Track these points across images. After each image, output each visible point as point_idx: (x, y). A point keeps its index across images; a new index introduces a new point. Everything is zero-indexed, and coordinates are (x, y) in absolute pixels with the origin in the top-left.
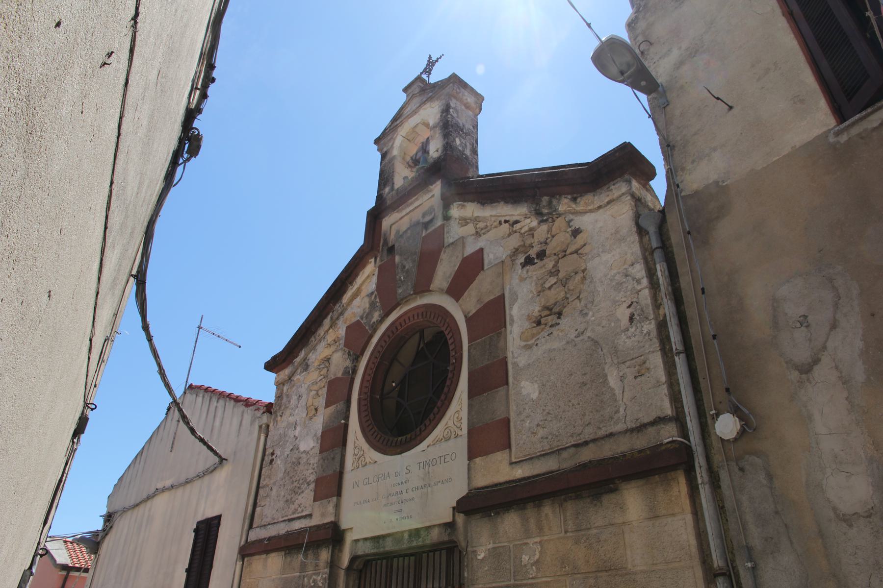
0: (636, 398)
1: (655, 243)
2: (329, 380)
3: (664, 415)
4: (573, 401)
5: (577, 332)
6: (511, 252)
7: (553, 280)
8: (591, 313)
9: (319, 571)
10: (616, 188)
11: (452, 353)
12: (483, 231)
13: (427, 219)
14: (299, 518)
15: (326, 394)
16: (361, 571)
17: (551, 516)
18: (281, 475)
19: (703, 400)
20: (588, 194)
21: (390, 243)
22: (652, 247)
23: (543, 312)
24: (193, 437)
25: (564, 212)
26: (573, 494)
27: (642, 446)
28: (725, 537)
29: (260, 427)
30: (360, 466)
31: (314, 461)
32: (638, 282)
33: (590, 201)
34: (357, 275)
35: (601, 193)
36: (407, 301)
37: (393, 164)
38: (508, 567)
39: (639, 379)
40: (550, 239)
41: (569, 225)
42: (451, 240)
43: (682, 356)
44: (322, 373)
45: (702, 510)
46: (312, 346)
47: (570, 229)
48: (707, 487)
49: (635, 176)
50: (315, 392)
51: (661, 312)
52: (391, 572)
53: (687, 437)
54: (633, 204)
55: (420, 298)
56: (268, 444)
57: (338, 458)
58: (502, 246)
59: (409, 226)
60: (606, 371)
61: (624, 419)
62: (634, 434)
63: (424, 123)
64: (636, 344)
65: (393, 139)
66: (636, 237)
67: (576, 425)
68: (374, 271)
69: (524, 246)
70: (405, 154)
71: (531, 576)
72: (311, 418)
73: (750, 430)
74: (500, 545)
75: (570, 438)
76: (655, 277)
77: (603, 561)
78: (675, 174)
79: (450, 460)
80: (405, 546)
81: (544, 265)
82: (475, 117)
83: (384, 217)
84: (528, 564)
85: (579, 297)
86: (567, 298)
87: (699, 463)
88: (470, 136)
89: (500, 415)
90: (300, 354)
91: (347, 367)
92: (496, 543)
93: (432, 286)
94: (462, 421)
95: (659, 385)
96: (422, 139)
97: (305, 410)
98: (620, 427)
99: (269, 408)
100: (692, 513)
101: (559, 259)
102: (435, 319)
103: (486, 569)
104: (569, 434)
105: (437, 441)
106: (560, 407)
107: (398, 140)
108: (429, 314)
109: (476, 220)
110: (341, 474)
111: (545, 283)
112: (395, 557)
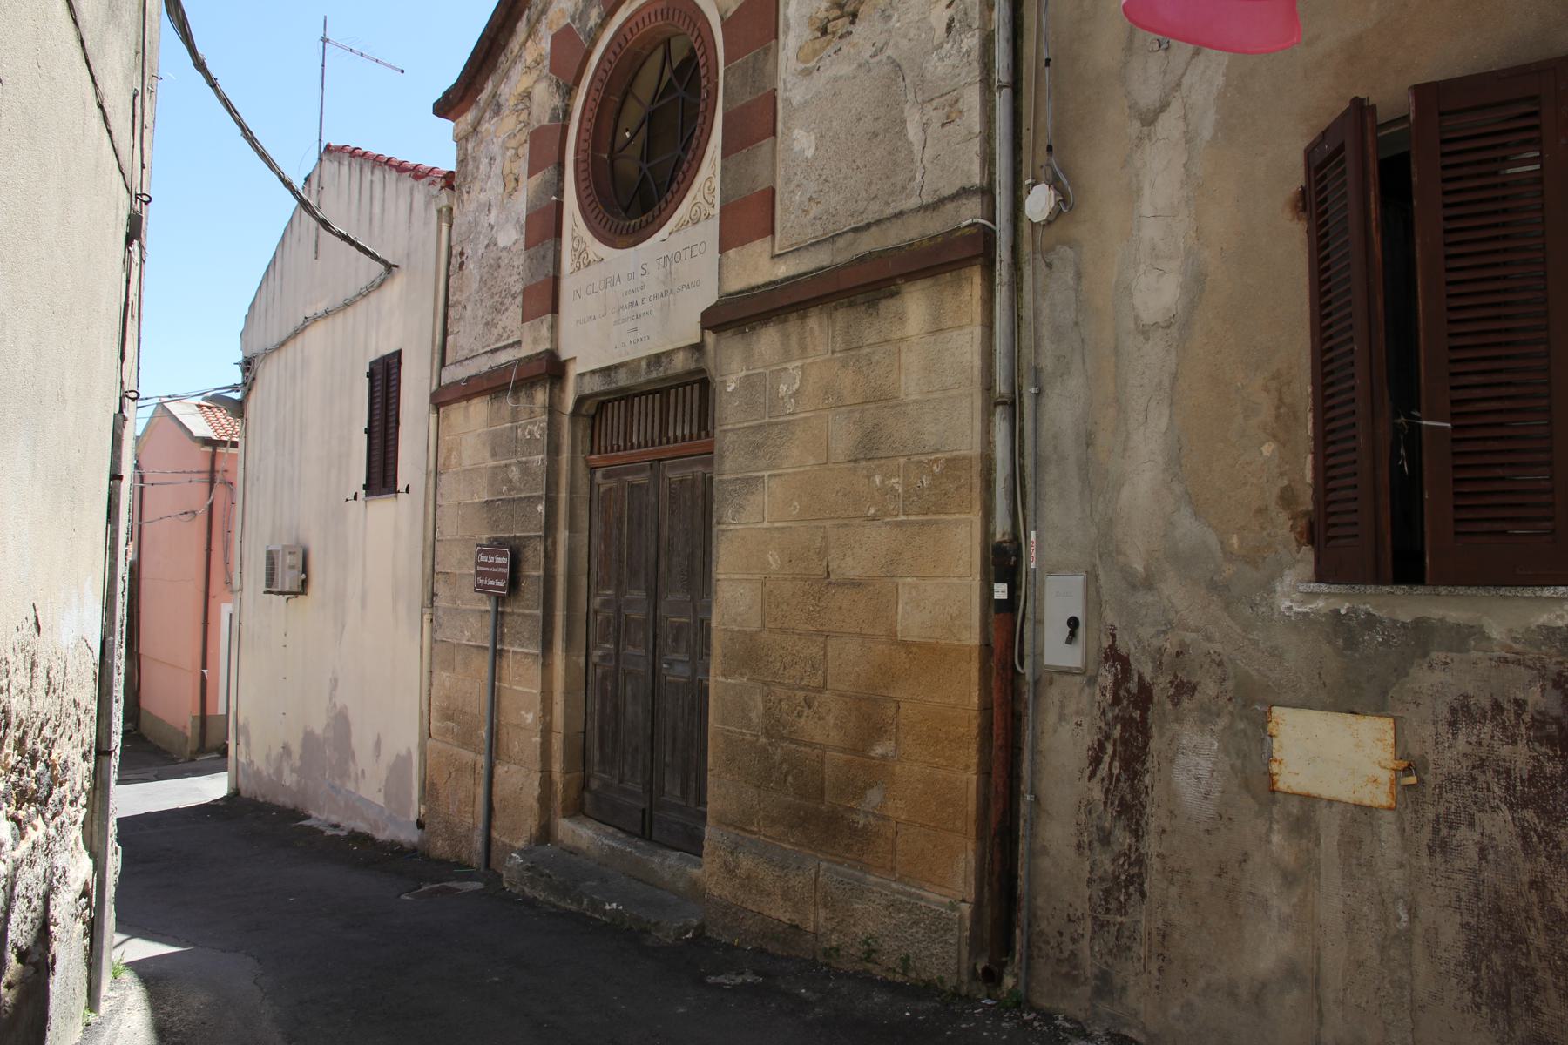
11: (704, 82)
14: (505, 347)
16: (593, 417)
17: (817, 330)
18: (475, 285)
24: (329, 233)
26: (846, 300)
29: (440, 211)
31: (519, 261)
38: (762, 401)
43: (1006, 92)
44: (521, 119)
48: (1004, 289)
50: (513, 151)
60: (906, 114)
62: (928, 212)
72: (510, 195)
74: (753, 372)
80: (642, 379)
91: (555, 109)
92: (749, 370)
97: (501, 182)
98: (914, 202)
99: (449, 180)
110: (556, 280)
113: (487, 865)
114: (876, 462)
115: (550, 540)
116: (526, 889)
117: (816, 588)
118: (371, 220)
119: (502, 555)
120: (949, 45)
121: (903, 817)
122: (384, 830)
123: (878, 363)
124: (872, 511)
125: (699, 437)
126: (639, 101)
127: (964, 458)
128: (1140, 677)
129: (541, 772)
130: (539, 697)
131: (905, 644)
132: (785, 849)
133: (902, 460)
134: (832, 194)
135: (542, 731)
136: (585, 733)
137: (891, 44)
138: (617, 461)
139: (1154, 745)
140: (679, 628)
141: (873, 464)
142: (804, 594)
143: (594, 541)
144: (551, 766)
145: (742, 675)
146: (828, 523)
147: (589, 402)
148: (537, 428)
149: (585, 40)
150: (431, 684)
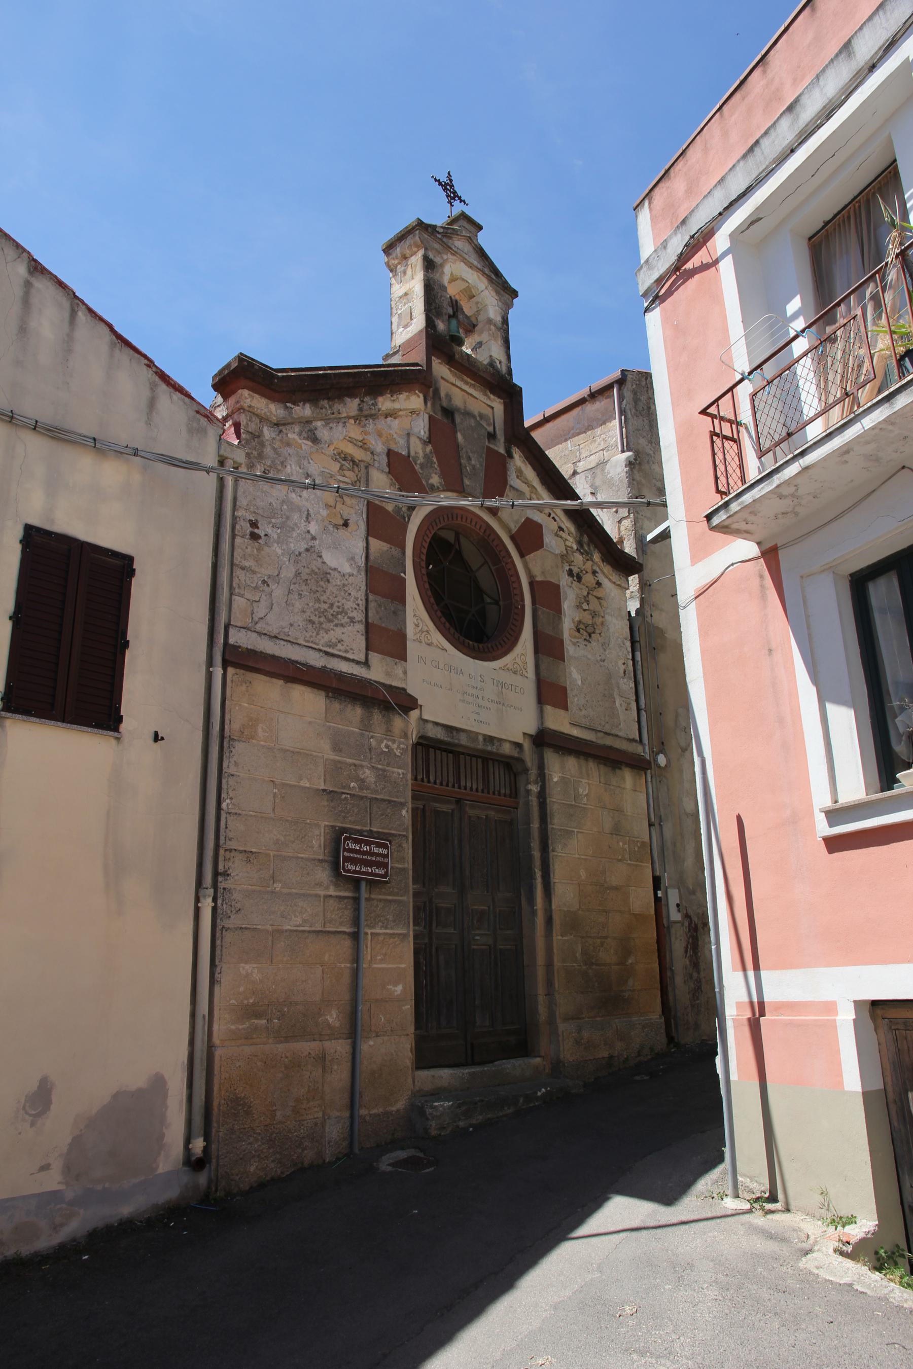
17: (593, 767)
103: (559, 789)
128: (695, 922)
139: (700, 943)
145: (571, 934)
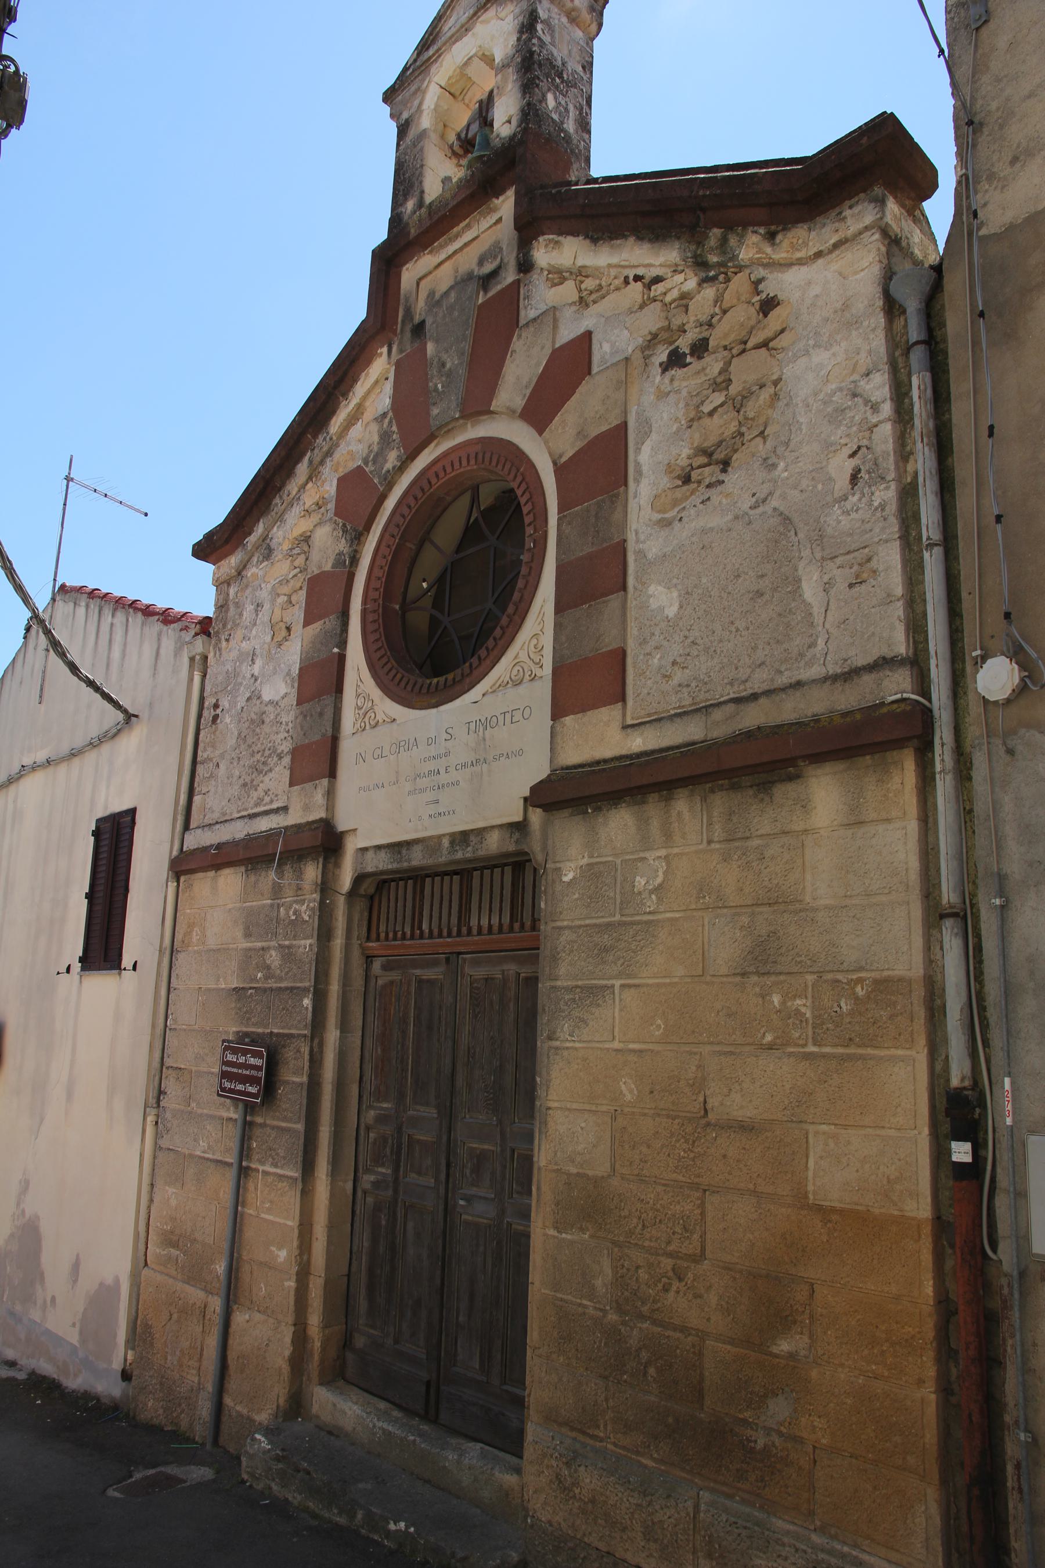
0: (847, 622)
1: (915, 332)
2: (309, 576)
3: (893, 655)
4: (738, 623)
5: (754, 499)
6: (643, 341)
7: (718, 398)
8: (782, 465)
9: (302, 897)
10: (852, 216)
11: (529, 531)
12: (594, 296)
13: (488, 268)
14: (266, 813)
15: (304, 601)
16: (372, 898)
17: (686, 815)
18: (232, 742)
19: (962, 632)
20: (800, 225)
21: (418, 317)
22: (908, 341)
23: (696, 459)
24: (76, 678)
25: (748, 263)
26: (726, 781)
27: (849, 706)
28: (967, 858)
29: (192, 659)
30: (368, 727)
31: (288, 717)
32: (875, 408)
33: (800, 241)
34: (355, 380)
35: (824, 225)
36: (449, 431)
37: (422, 150)
38: (612, 895)
39: (857, 589)
40: (718, 317)
41: (756, 288)
42: (532, 314)
43: (938, 551)
44: (296, 563)
45: (937, 815)
46: (277, 513)
47: (758, 298)
48: (949, 778)
49: (893, 188)
50: (286, 598)
51: (910, 468)
52: (422, 900)
53: (926, 694)
54: (883, 249)
55: (472, 426)
56: (208, 688)
57: (329, 713)
58: (626, 328)
59: (453, 283)
60: (800, 572)
61: (822, 659)
62: (838, 684)
63: (483, 54)
64: (857, 525)
65: (420, 91)
66: (881, 320)
67: (739, 664)
68: (388, 371)
69: (668, 329)
70: (445, 126)
71: (648, 910)
72: (280, 645)
73: (1036, 686)
74: (598, 860)
75: (728, 687)
76: (906, 401)
77: (767, 890)
78: (974, 188)
79: (522, 719)
80: (443, 859)
81: (704, 369)
82: (587, 44)
83: (406, 262)
84: (644, 890)
85: (762, 432)
86: (742, 435)
87: (941, 738)
88: (576, 88)
89: (609, 643)
90: (255, 529)
91: (340, 554)
92: (592, 857)
93: (494, 403)
94: (544, 652)
95: (891, 602)
96: (478, 94)
97: (268, 630)
98: (815, 671)
99: (205, 626)
100: (918, 819)
101: (733, 357)
102: (500, 467)
103: (576, 896)
104: (726, 681)
105: (500, 685)
106: (714, 632)
107: (432, 96)
108: (487, 456)
109: (580, 273)
110: (335, 740)
111: (702, 402)
112: (428, 876)
113: (216, 1442)
114: (773, 978)
115: (316, 1041)
116: (275, 1487)
117: (689, 1129)
118: (108, 665)
119: (257, 1055)
120: (856, 497)
121: (824, 1441)
122: (76, 1376)
123: (773, 858)
124: (769, 1038)
125: (511, 929)
126: (437, 547)
127: (900, 979)
129: (295, 1325)
130: (296, 1231)
131: (819, 1209)
132: (646, 1467)
133: (810, 978)
134: (703, 658)
135: (298, 1274)
136: (349, 1275)
137: (777, 493)
138: (402, 951)
140: (480, 1159)
141: (769, 980)
142: (672, 1135)
143: (369, 1043)
144: (306, 1318)
145: (582, 1230)
146: (706, 1049)
147: (369, 880)
148: (306, 909)
149: (380, 483)
150: (151, 1201)
